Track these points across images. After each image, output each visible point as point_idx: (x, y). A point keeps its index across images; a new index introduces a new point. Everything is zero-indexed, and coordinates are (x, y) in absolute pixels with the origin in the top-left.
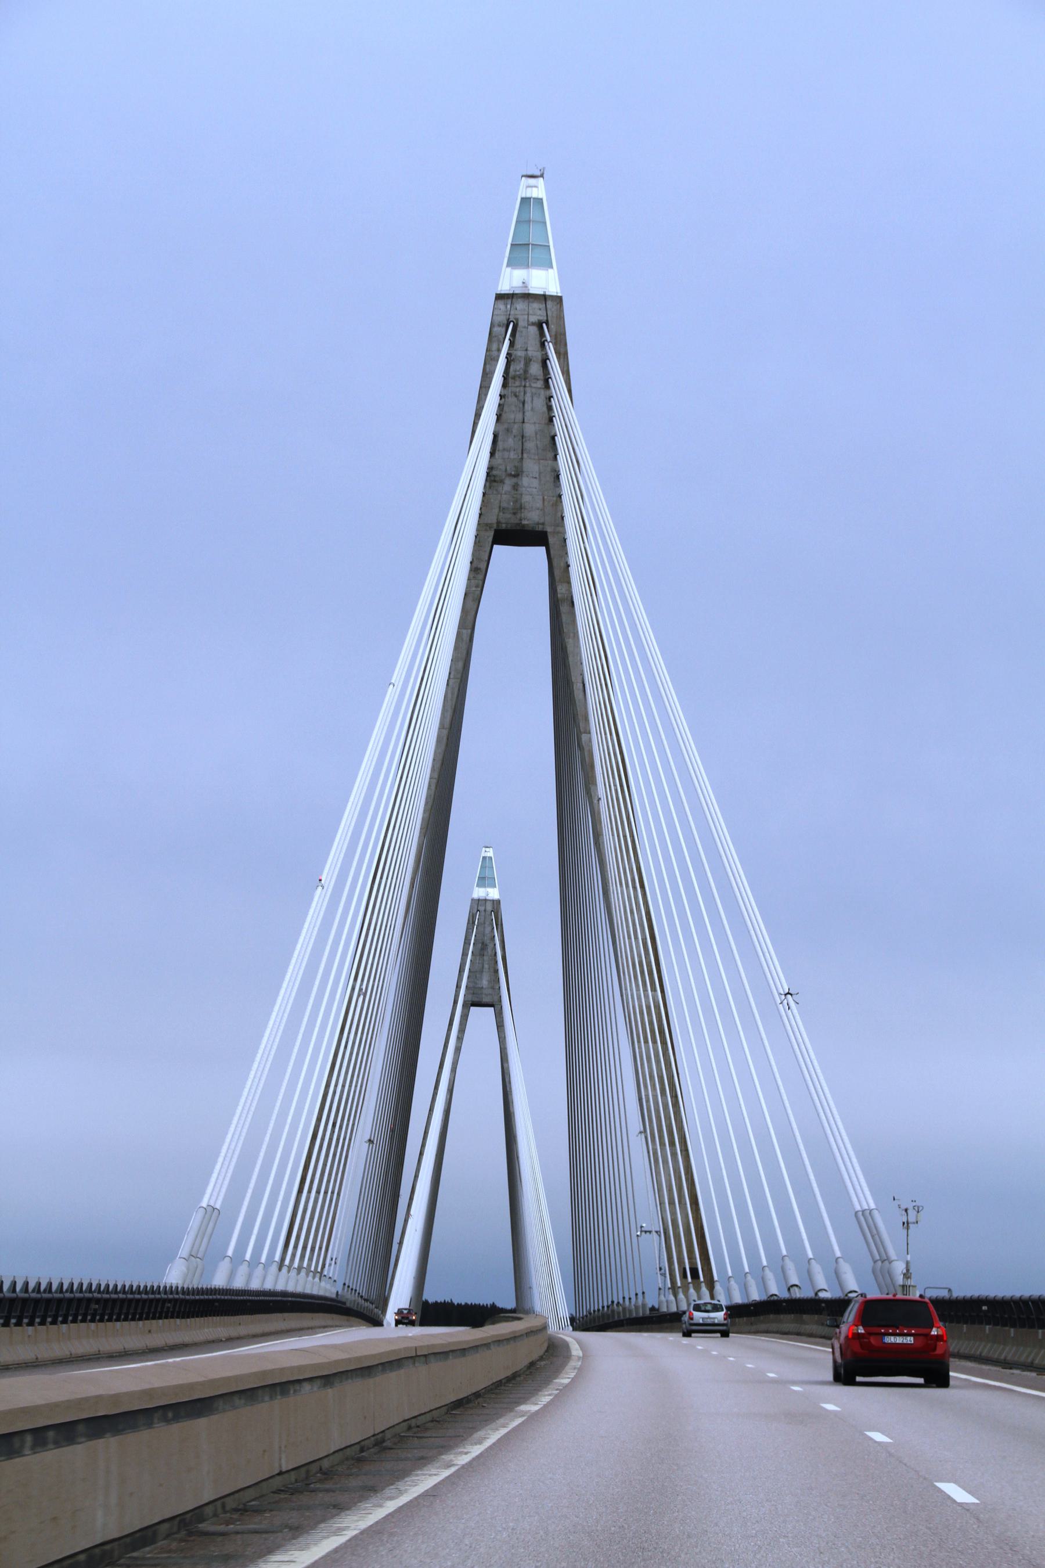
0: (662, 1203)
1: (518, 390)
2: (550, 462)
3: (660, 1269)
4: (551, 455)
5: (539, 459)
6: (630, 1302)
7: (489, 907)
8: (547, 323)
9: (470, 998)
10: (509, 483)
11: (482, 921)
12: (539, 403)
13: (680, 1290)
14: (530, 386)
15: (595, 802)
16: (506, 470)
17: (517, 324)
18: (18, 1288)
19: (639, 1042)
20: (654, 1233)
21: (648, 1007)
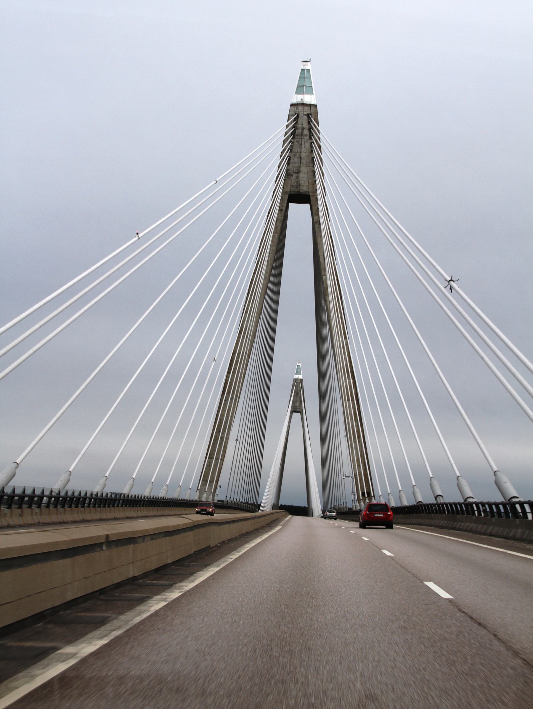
0: (354, 466)
1: (299, 140)
2: (311, 168)
3: (353, 492)
4: (312, 165)
5: (307, 167)
6: (341, 506)
7: (299, 381)
8: (311, 114)
9: (293, 409)
10: (295, 176)
11: (297, 385)
12: (307, 145)
13: (362, 501)
14: (304, 139)
15: (328, 302)
16: (294, 171)
17: (299, 115)
18: (133, 497)
19: (345, 400)
20: (351, 478)
21: (350, 386)
